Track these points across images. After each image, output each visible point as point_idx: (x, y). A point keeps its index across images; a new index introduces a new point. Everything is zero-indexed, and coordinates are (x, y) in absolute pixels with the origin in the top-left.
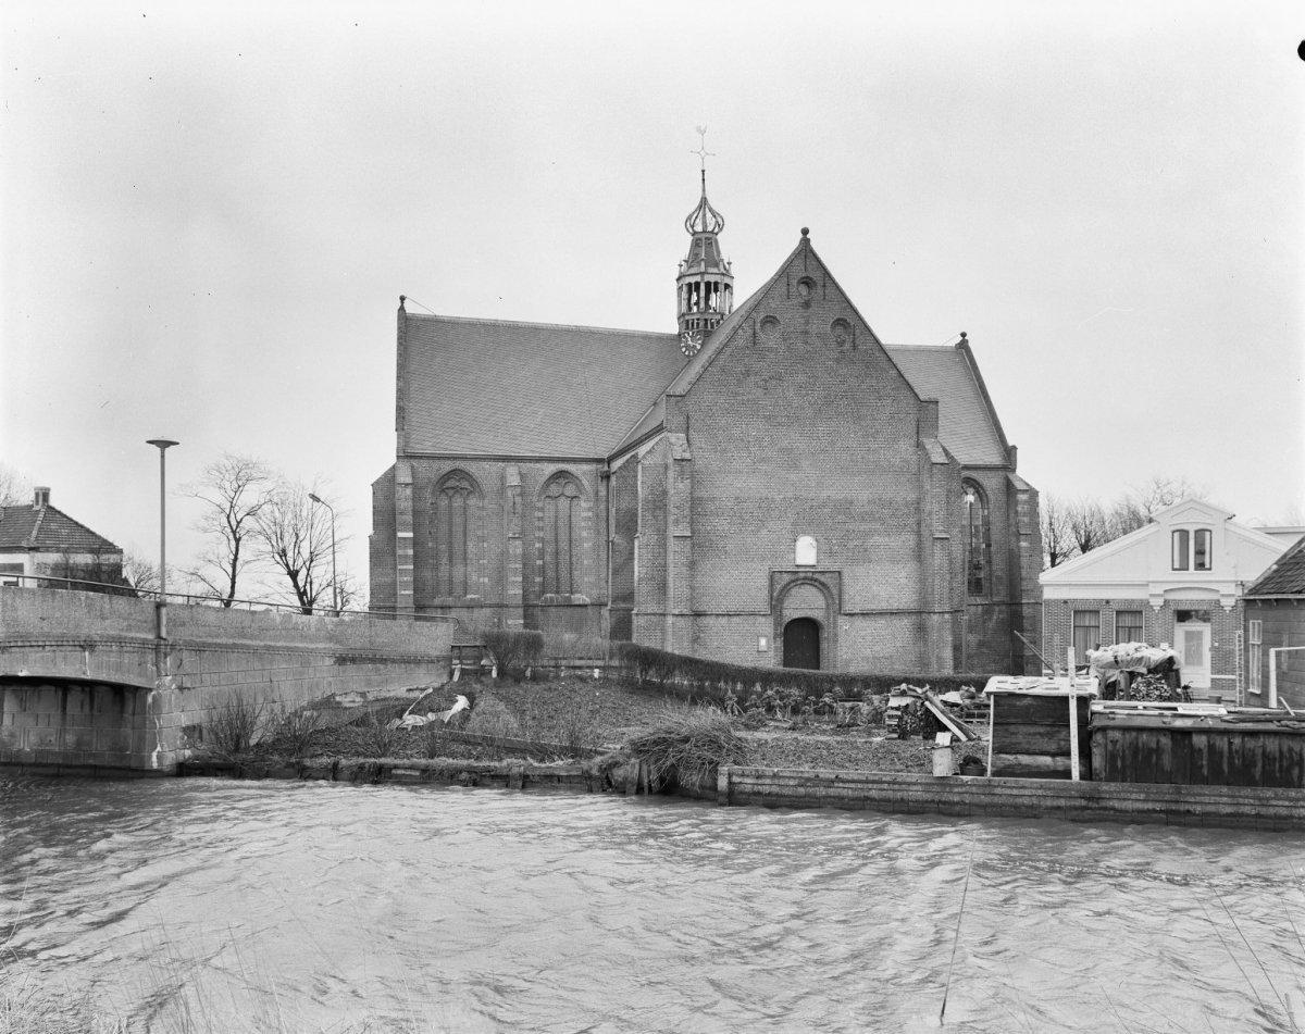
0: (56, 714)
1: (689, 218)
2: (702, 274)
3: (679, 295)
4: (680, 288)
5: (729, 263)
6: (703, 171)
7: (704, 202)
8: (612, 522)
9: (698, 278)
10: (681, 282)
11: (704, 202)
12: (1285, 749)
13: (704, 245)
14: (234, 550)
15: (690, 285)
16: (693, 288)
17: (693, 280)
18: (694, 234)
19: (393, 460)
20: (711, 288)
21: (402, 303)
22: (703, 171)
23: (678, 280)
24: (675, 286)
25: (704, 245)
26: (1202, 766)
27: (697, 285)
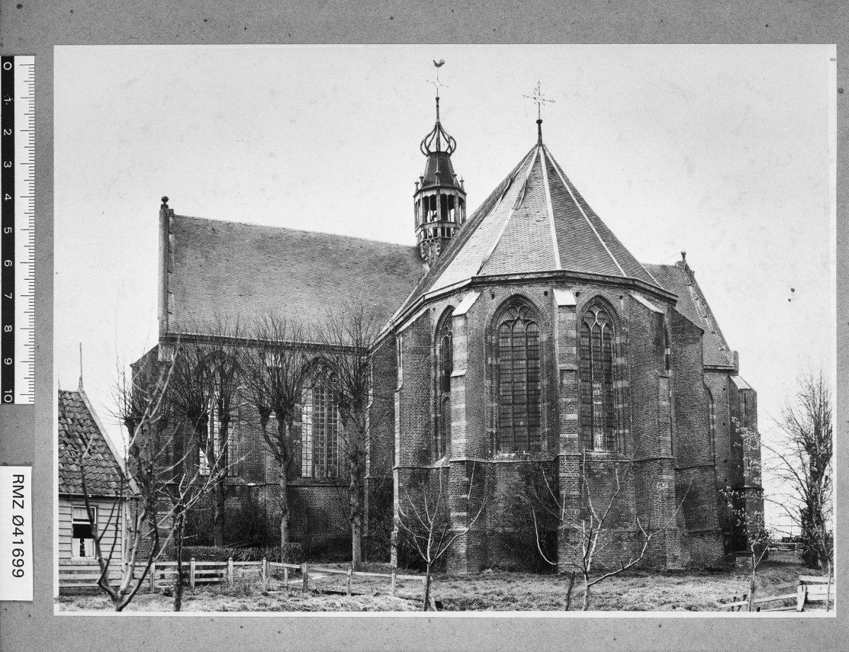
0: (90, 475)
1: (425, 141)
2: (437, 188)
3: (416, 211)
4: (417, 204)
5: (462, 181)
6: (539, 122)
7: (438, 127)
8: (557, 170)
9: (435, 193)
10: (418, 197)
11: (438, 127)
12: (508, 416)
13: (440, 163)
14: (547, 153)
15: (426, 199)
16: (429, 204)
17: (429, 194)
18: (430, 154)
19: (154, 341)
20: (448, 203)
21: (437, 101)
22: (539, 122)
23: (415, 196)
24: (411, 202)
25: (440, 163)
26: (472, 521)
27: (433, 197)
